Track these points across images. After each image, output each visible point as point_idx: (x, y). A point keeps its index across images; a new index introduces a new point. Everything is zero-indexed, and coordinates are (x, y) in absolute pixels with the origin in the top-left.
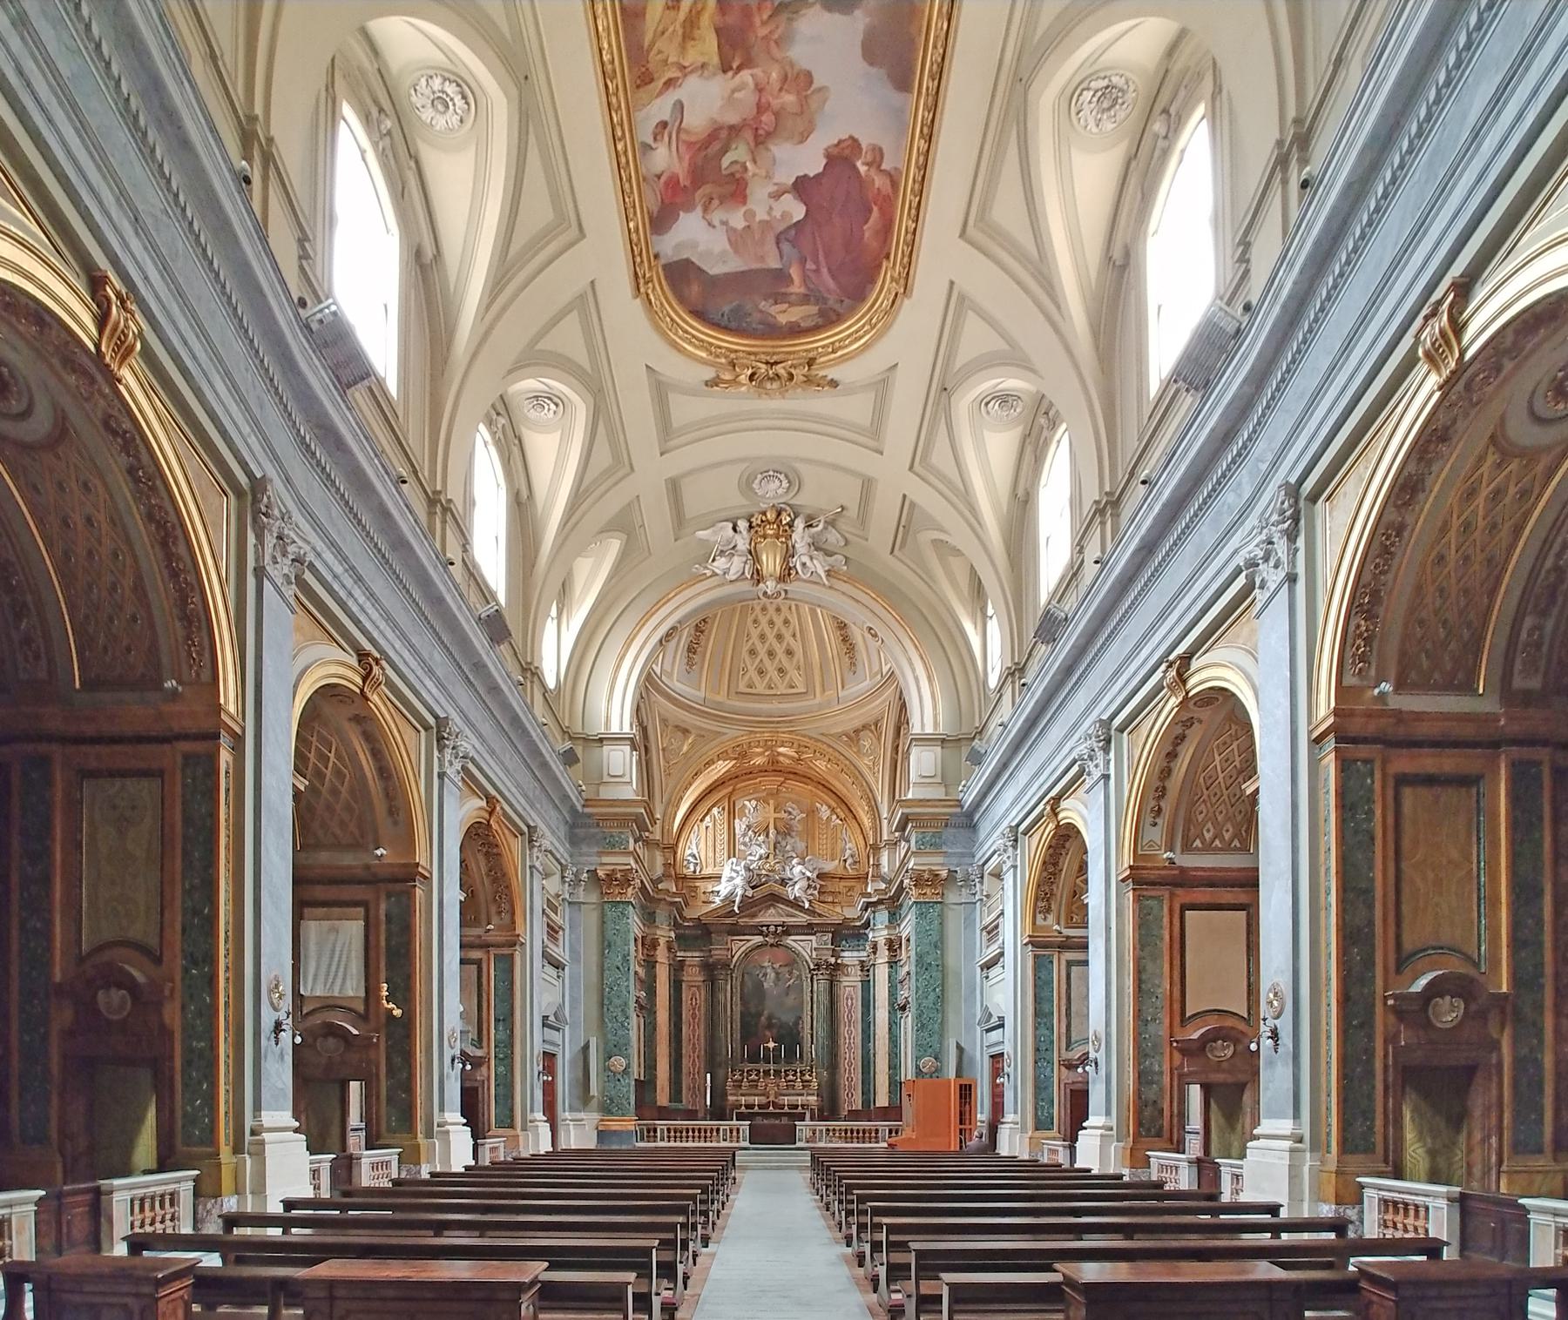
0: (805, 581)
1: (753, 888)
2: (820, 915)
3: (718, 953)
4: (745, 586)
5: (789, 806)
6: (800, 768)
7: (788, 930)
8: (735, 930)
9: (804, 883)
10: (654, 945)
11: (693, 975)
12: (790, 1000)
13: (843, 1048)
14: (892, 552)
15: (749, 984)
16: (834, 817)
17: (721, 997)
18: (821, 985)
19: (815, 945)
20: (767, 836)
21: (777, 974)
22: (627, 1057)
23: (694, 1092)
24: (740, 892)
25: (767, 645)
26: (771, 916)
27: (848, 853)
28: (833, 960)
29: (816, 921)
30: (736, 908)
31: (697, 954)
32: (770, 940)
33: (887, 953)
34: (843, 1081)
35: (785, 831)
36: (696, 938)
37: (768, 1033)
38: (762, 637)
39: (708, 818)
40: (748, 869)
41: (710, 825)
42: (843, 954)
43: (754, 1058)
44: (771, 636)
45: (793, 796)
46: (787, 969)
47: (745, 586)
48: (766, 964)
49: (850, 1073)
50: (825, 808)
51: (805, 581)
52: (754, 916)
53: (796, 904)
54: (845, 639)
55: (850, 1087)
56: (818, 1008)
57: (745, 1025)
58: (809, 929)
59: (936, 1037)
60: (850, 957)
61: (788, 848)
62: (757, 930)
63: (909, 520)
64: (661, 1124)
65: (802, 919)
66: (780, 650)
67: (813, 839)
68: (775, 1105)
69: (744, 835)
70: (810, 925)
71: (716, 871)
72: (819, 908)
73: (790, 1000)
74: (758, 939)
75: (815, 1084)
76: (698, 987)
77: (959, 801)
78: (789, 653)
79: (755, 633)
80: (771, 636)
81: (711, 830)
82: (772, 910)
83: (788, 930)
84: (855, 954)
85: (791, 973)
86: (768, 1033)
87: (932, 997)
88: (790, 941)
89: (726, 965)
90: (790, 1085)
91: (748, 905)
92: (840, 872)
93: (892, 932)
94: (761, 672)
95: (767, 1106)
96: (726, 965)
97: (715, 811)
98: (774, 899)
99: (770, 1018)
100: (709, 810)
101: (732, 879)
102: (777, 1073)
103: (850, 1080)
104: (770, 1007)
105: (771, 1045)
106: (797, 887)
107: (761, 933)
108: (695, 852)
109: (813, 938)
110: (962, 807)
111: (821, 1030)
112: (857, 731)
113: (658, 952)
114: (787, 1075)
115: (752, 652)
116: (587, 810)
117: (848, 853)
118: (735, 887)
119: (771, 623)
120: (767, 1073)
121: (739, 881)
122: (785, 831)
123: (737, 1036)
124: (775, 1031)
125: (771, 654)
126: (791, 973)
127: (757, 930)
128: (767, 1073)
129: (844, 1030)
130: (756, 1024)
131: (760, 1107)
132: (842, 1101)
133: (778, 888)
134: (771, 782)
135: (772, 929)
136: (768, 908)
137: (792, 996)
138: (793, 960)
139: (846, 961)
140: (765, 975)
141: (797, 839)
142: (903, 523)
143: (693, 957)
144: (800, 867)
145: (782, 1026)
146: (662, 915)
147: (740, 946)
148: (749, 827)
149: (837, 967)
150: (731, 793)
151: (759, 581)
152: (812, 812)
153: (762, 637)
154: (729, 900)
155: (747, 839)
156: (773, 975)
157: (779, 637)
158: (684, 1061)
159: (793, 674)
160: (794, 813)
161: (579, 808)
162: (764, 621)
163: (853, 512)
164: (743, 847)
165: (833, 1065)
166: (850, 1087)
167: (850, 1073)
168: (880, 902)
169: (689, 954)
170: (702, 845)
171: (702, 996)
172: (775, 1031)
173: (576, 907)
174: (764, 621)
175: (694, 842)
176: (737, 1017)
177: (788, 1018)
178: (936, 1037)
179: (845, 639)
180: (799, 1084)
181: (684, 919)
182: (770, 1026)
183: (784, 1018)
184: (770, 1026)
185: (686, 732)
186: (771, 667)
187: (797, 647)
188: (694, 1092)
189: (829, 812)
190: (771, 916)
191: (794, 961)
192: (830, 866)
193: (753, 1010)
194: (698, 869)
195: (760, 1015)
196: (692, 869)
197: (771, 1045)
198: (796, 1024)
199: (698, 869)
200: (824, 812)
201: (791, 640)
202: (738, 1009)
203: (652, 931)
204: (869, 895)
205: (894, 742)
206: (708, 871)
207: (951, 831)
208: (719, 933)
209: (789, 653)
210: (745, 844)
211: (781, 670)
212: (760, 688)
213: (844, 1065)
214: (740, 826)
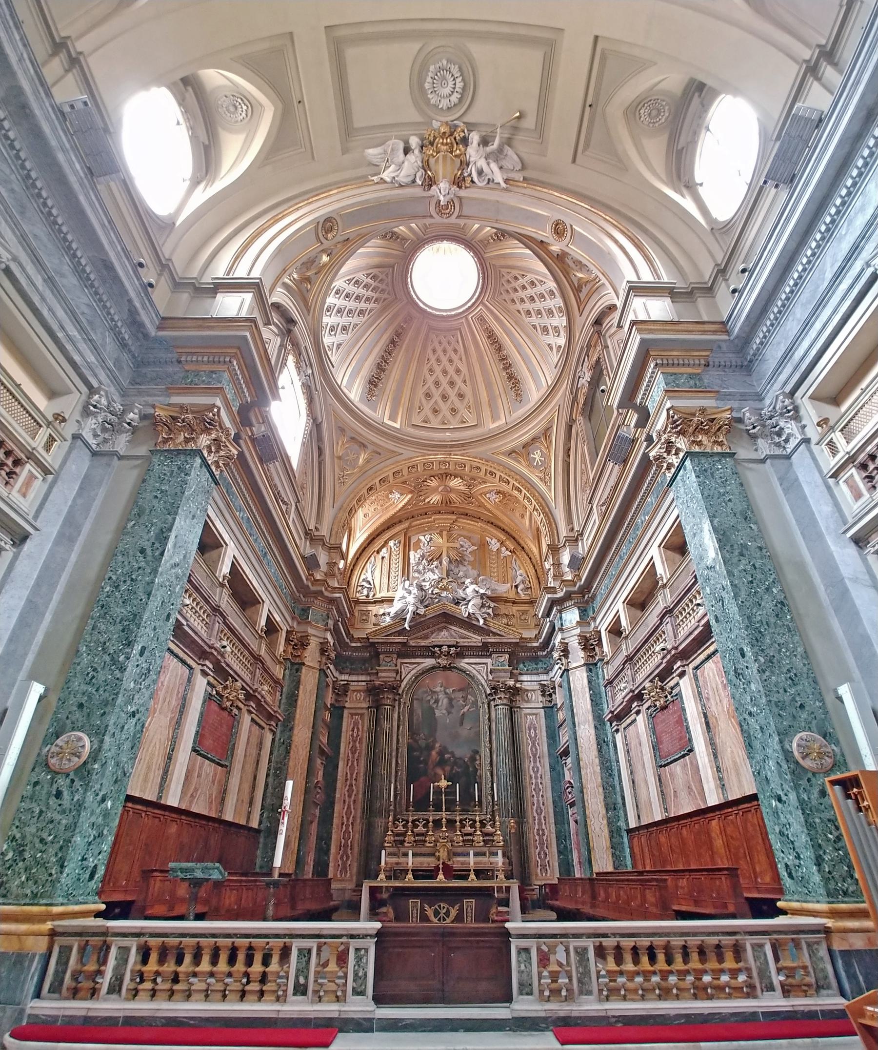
0: (481, 188)
1: (426, 606)
2: (495, 634)
3: (386, 675)
4: (418, 192)
5: (462, 541)
6: (471, 508)
7: (462, 652)
8: (406, 652)
9: (478, 601)
10: (303, 643)
11: (356, 701)
12: (465, 731)
13: (529, 792)
14: (574, 161)
15: (419, 712)
16: (503, 549)
17: (386, 725)
18: (500, 712)
19: (490, 667)
20: (441, 563)
21: (451, 700)
22: (99, 733)
23: (345, 852)
24: (411, 608)
25: (441, 389)
26: (444, 637)
27: (519, 579)
28: (511, 683)
29: (491, 639)
30: (406, 626)
31: (363, 678)
32: (443, 662)
33: (582, 654)
34: (533, 836)
35: (459, 561)
36: (364, 661)
37: (439, 771)
38: (437, 384)
39: (384, 550)
40: (421, 588)
41: (387, 556)
42: (524, 678)
43: (421, 804)
44: (444, 382)
45: (465, 533)
46: (460, 694)
47: (418, 192)
48: (438, 689)
49: (540, 824)
50: (494, 541)
51: (481, 188)
52: (426, 637)
53: (468, 624)
54: (511, 377)
55: (542, 844)
56: (498, 738)
57: (412, 762)
58: (484, 650)
59: (805, 685)
60: (529, 681)
61: (461, 574)
62: (428, 651)
63: (597, 95)
64: (473, 881)
65: (476, 639)
66: (452, 394)
67: (485, 567)
68: (450, 873)
69: (418, 564)
70: (485, 645)
71: (390, 594)
72: (495, 625)
73: (465, 731)
74: (429, 662)
75: (499, 838)
76: (362, 715)
77: (723, 324)
78: (461, 396)
79: (430, 380)
80: (444, 382)
81: (386, 560)
82: (445, 633)
83: (462, 652)
84: (535, 678)
85: (465, 699)
86: (439, 771)
87: (768, 604)
88: (463, 663)
89: (394, 688)
90: (469, 842)
91: (420, 624)
92: (512, 595)
93: (586, 629)
94: (435, 411)
95: (431, 874)
96: (394, 688)
97: (391, 543)
98: (447, 619)
99: (441, 753)
100: (386, 542)
101: (404, 597)
102: (451, 823)
103: (541, 832)
104: (442, 739)
105: (444, 783)
106: (471, 604)
107: (433, 655)
108: (370, 579)
109: (488, 661)
110: (727, 332)
111: (503, 767)
112: (525, 446)
113: (307, 653)
114: (463, 826)
115: (428, 395)
116: (161, 333)
117: (519, 579)
118: (407, 604)
119: (445, 372)
120: (437, 823)
121: (411, 599)
122: (459, 561)
123: (403, 774)
124: (448, 768)
125: (444, 397)
126: (465, 699)
127: (428, 651)
128: (437, 823)
129: (528, 767)
130: (426, 762)
131: (418, 874)
132: (532, 864)
133: (451, 608)
134: (445, 520)
135: (445, 649)
136: (441, 630)
137: (467, 725)
138: (468, 683)
139: (526, 686)
140: (437, 701)
141: (470, 567)
142: (589, 102)
143: (358, 681)
144: (474, 586)
145: (457, 761)
146: (317, 610)
147: (410, 669)
148: (423, 557)
149: (515, 692)
150: (407, 529)
151: (431, 186)
152: (483, 546)
153: (437, 384)
154: (400, 617)
155: (421, 568)
156: (446, 701)
157: (452, 384)
158: (337, 808)
159: (464, 412)
160: (466, 545)
161: (152, 332)
162: (438, 370)
163: (529, 123)
164: (416, 575)
165: (520, 813)
166: (542, 844)
167: (540, 824)
168: (568, 597)
169: (354, 678)
170: (377, 573)
171: (365, 724)
172: (448, 768)
173: (105, 460)
174: (438, 370)
175: (369, 571)
176: (404, 751)
177: (462, 752)
178: (805, 685)
179: (511, 377)
180: (479, 838)
181: (352, 639)
182: (442, 763)
183: (459, 753)
184: (442, 763)
185: (363, 446)
186: (444, 408)
187: (467, 390)
188: (345, 852)
189: (498, 544)
190: (444, 637)
191: (469, 686)
192: (503, 589)
193: (422, 743)
194: (371, 594)
195: (430, 748)
196: (365, 592)
197: (444, 783)
198: (473, 759)
199: (371, 594)
200: (494, 545)
201: (463, 385)
202: (405, 740)
203: (301, 628)
204: (553, 590)
205: (565, 444)
206: (384, 594)
207: (713, 372)
208: (389, 653)
209: (461, 396)
210: (419, 572)
211: (454, 410)
212: (435, 422)
213: (531, 812)
214: (414, 556)
